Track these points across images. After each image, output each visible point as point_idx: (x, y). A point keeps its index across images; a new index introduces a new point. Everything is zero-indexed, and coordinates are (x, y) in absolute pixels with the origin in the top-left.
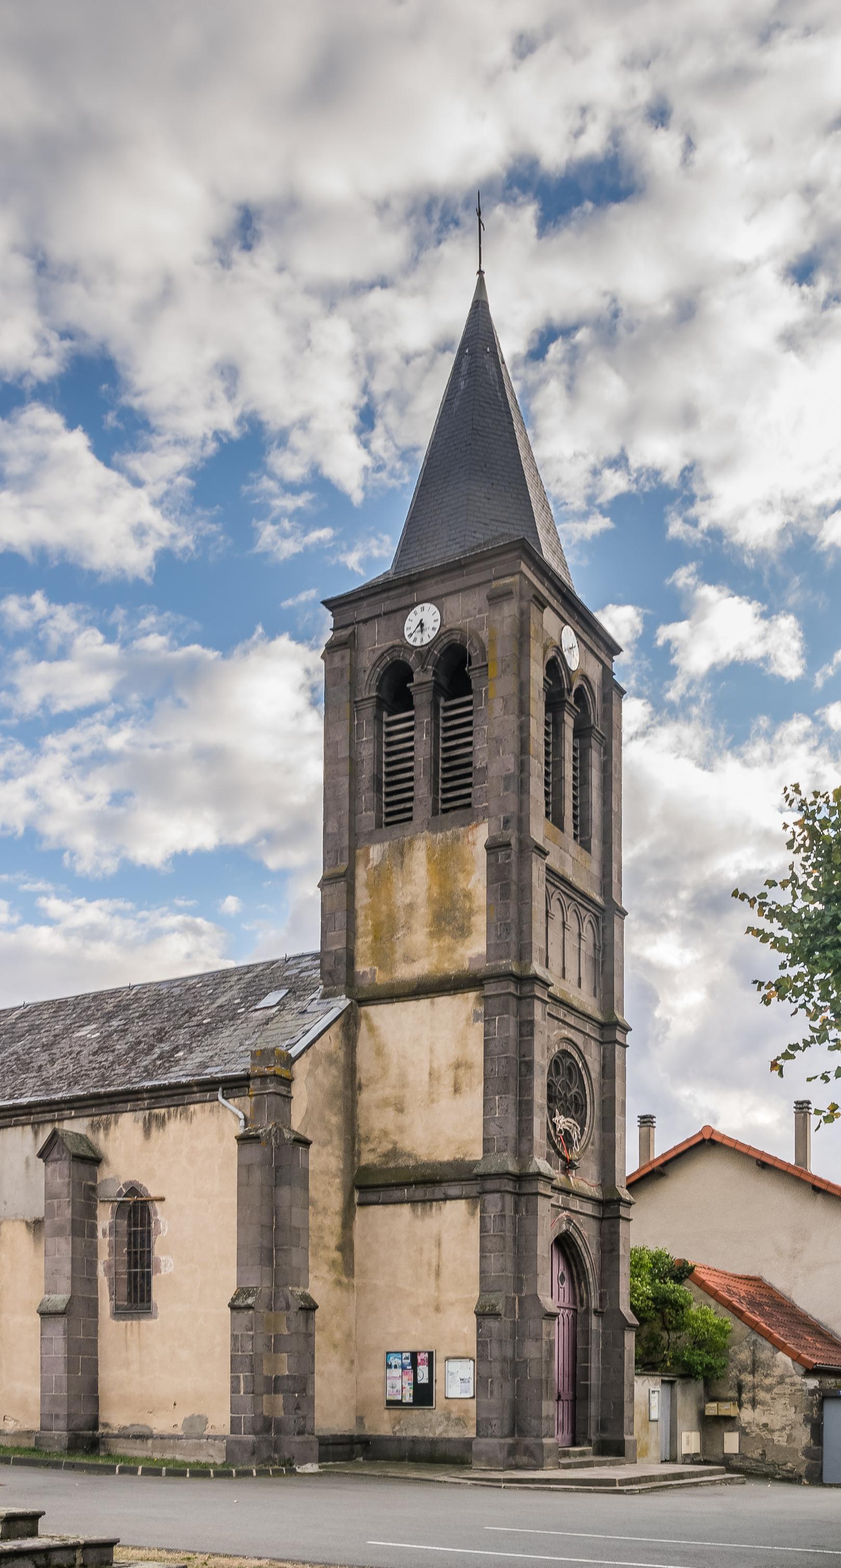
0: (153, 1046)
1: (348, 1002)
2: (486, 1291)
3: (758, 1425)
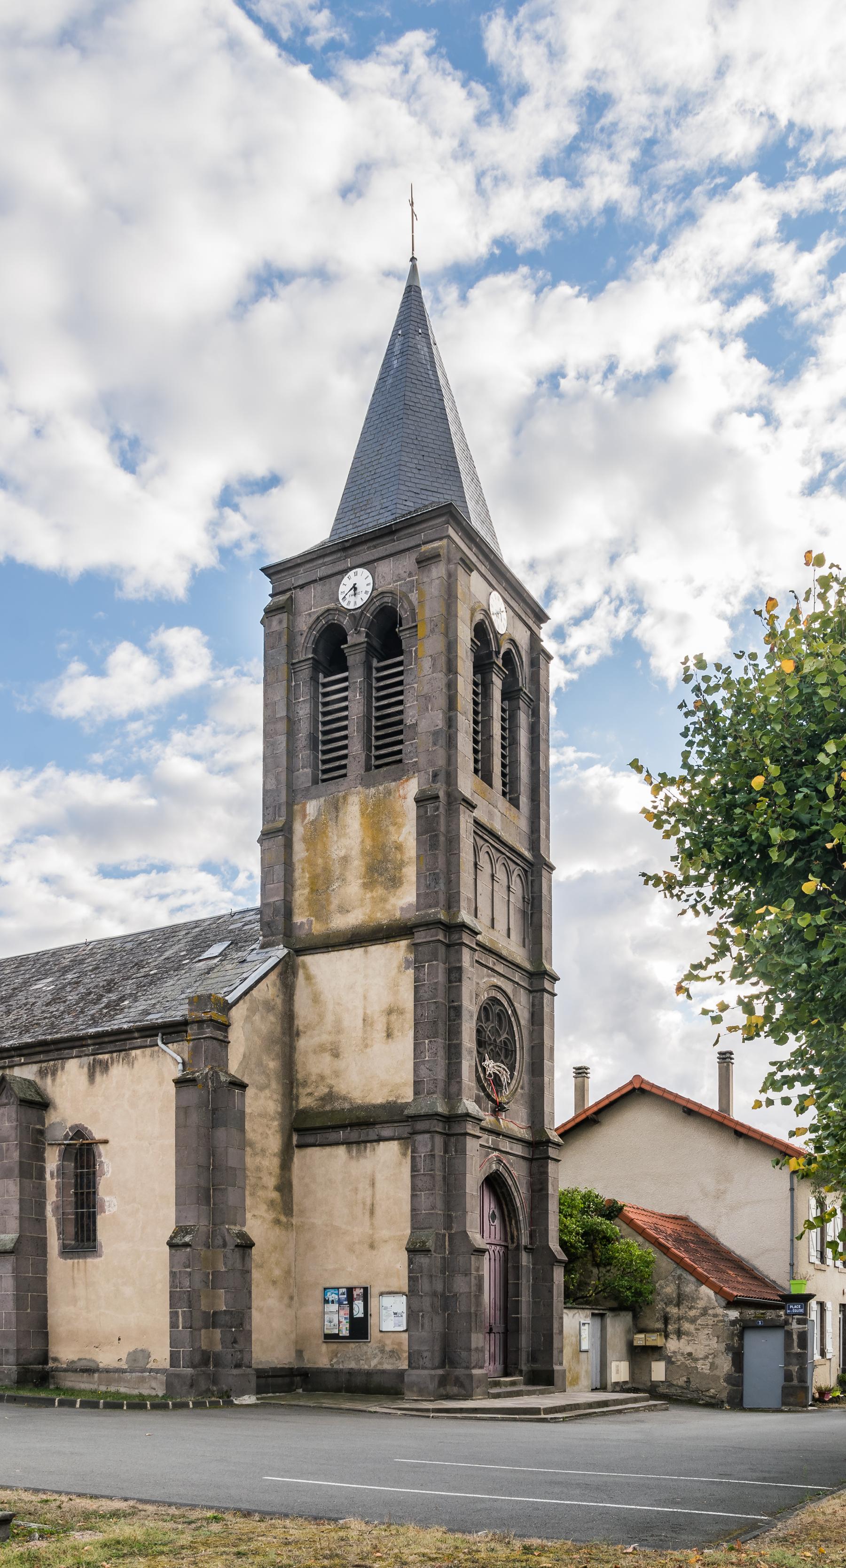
0: (102, 996)
1: (286, 951)
2: (417, 1229)
3: (682, 1354)
